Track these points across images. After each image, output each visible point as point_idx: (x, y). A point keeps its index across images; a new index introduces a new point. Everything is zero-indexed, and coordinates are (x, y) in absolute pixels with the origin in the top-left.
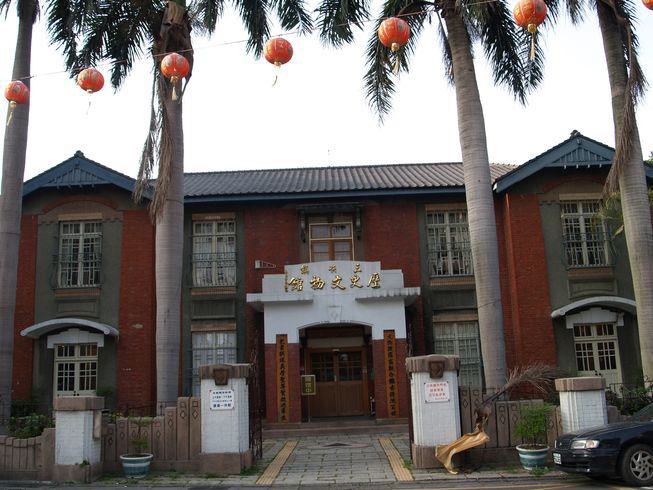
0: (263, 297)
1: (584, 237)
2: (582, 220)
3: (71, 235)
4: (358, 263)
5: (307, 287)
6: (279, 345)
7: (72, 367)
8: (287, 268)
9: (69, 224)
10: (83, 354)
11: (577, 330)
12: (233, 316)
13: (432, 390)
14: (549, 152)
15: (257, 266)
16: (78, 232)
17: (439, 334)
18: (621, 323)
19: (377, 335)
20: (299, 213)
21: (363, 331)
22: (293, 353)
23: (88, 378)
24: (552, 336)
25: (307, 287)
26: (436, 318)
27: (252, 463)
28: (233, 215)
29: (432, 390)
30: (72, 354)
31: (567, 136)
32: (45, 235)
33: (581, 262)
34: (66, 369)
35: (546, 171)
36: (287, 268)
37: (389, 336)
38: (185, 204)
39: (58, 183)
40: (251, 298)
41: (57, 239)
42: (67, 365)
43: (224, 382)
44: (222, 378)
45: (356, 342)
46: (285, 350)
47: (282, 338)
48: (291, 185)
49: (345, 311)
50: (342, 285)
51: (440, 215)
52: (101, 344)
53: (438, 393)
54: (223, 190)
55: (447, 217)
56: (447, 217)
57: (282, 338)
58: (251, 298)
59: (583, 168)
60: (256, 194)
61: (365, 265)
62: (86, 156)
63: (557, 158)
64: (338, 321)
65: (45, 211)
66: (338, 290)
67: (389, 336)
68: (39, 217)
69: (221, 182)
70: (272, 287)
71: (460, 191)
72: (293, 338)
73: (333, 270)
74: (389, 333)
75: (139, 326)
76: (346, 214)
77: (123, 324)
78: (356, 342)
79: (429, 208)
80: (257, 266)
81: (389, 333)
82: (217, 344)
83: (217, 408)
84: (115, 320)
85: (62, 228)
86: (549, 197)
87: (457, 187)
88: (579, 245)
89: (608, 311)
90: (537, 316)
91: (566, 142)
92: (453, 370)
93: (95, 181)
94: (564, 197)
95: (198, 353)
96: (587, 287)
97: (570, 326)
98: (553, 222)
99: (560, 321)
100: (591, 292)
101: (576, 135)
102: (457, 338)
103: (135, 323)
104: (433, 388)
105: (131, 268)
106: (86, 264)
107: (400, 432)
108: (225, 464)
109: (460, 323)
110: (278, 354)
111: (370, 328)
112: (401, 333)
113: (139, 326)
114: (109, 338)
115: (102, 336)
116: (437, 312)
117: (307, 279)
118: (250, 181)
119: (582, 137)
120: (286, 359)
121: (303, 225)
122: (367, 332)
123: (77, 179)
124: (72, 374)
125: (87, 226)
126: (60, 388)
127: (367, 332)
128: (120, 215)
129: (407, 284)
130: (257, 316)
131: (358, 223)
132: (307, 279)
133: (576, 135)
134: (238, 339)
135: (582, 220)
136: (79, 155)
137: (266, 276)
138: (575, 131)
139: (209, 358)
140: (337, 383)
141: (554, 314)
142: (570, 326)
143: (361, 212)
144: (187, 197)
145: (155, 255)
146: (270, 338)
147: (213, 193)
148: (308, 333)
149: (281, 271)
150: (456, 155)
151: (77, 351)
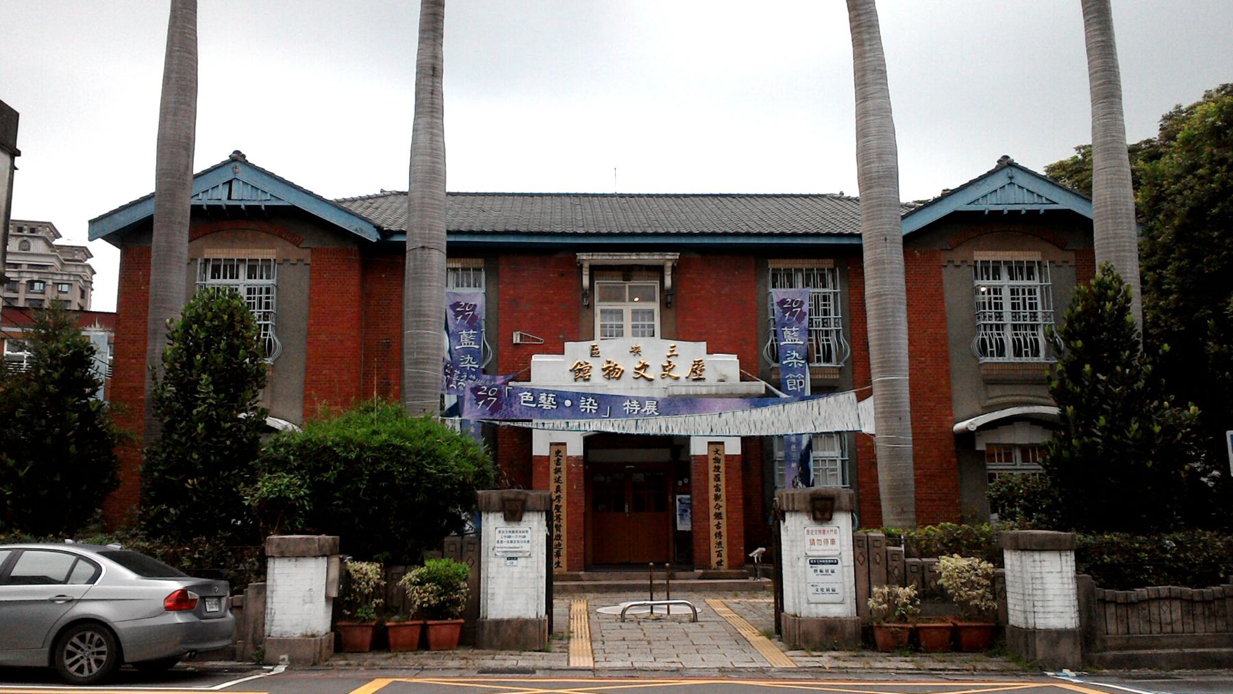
1: (1007, 319)
2: (1006, 293)
4: (673, 343)
6: (554, 459)
11: (988, 455)
15: (516, 338)
19: (698, 448)
21: (678, 445)
24: (954, 460)
28: (479, 262)
31: (992, 166)
35: (956, 218)
36: (567, 345)
43: (827, 515)
44: (822, 509)
45: (663, 455)
46: (563, 466)
47: (558, 447)
48: (385, 220)
50: (674, 374)
57: (558, 447)
59: (1014, 214)
60: (516, 233)
63: (985, 192)
67: (558, 452)
71: (855, 241)
73: (636, 351)
79: (772, 264)
80: (516, 338)
84: (297, 413)
86: (959, 255)
87: (851, 235)
90: (931, 430)
92: (846, 511)
93: (261, 200)
99: (967, 437)
105: (323, 337)
106: (1015, 327)
107: (755, 589)
117: (597, 366)
119: (1016, 166)
123: (242, 196)
128: (305, 254)
132: (597, 366)
135: (1006, 293)
137: (536, 358)
138: (1006, 157)
140: (638, 515)
141: (959, 426)
142: (981, 447)
144: (449, 233)
145: (864, 312)
150: (843, 179)
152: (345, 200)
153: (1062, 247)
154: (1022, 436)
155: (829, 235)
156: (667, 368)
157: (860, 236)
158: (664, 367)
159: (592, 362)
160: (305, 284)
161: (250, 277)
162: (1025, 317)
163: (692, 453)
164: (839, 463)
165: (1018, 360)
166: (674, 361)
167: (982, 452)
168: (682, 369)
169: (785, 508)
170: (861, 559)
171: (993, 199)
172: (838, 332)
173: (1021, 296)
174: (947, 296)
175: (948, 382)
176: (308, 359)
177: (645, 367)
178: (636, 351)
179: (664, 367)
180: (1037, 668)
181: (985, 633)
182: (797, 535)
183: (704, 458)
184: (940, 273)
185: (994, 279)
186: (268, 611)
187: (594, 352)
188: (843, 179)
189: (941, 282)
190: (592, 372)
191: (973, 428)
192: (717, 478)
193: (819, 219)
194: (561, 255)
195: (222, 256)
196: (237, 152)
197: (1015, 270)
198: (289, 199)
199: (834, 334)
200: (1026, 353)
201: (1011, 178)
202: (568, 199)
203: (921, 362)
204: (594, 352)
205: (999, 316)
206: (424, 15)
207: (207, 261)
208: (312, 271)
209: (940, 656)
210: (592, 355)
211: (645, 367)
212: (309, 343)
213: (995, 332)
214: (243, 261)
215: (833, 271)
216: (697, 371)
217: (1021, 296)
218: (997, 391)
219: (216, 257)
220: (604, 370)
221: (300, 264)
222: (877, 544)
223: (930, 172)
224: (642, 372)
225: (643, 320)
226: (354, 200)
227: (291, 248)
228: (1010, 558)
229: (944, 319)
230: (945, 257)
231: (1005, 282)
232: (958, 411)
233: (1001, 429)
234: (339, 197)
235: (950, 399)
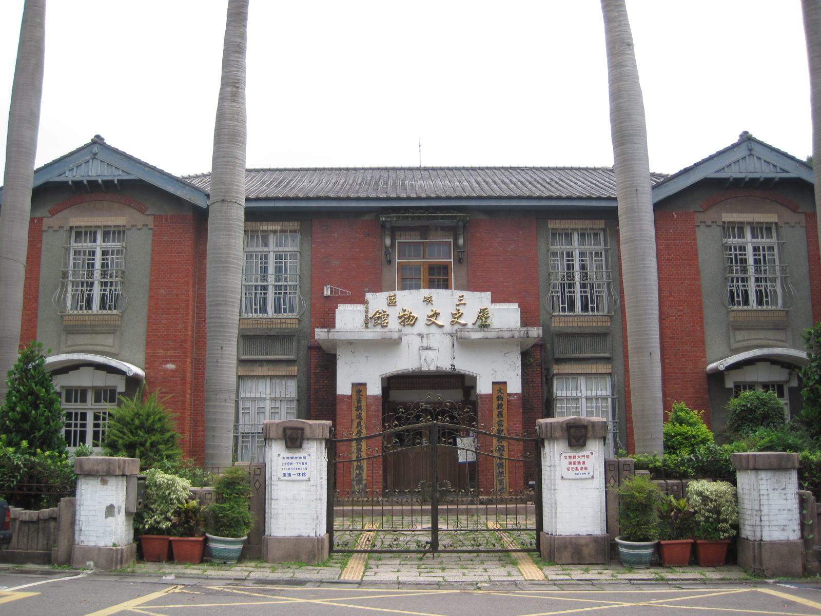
0: (334, 335)
3: (86, 245)
5: (393, 323)
6: (355, 397)
7: (84, 416)
8: (369, 296)
9: (83, 230)
10: (97, 400)
12: (292, 357)
13: (570, 463)
14: (711, 158)
15: (327, 292)
16: (95, 241)
17: (561, 391)
18: (794, 383)
19: (484, 388)
20: (383, 226)
21: (462, 383)
22: (373, 408)
23: (75, 432)
24: (707, 396)
25: (393, 323)
26: (556, 369)
27: (328, 549)
28: (296, 225)
29: (570, 463)
30: (84, 400)
31: (735, 139)
32: (51, 242)
33: (746, 302)
34: (76, 419)
36: (369, 296)
37: (500, 390)
38: (246, 208)
39: (70, 177)
40: (320, 334)
41: (67, 250)
42: (76, 414)
43: (581, 441)
45: (450, 397)
46: (363, 404)
47: (359, 388)
49: (440, 357)
50: (439, 322)
51: (119, 232)
52: (121, 388)
53: (579, 466)
54: (285, 192)
55: (576, 237)
56: (576, 237)
57: (359, 388)
58: (320, 334)
59: (753, 181)
60: (328, 198)
61: (468, 295)
62: (108, 142)
64: (433, 368)
65: (53, 213)
66: (424, 327)
67: (359, 392)
68: (45, 220)
69: (280, 183)
70: (349, 319)
72: (375, 389)
73: (428, 300)
74: (500, 386)
75: (171, 366)
76: (444, 229)
77: (148, 365)
78: (450, 397)
79: (553, 224)
80: (327, 292)
81: (500, 386)
82: (271, 398)
83: (287, 478)
84: (141, 357)
85: (73, 234)
86: (710, 215)
87: (609, 199)
88: (744, 280)
89: (779, 367)
90: (688, 371)
91: (734, 146)
93: (115, 175)
94: (728, 217)
95: (248, 405)
96: (753, 334)
97: (729, 384)
98: (708, 245)
99: (717, 377)
100: (746, 344)
101: (746, 138)
102: (268, 402)
103: (167, 362)
104: (572, 460)
105: (162, 291)
106: (757, 280)
108: (304, 552)
109: (586, 375)
110: (354, 409)
111: (474, 379)
112: (515, 386)
113: (171, 366)
114: (133, 382)
115: (124, 378)
116: (559, 361)
117: (394, 314)
118: (293, 184)
120: (364, 415)
121: (388, 242)
122: (467, 384)
123: (96, 171)
124: (83, 426)
125: (753, 230)
126: (604, 425)
127: (467, 384)
128: (150, 221)
129: (525, 322)
130: (324, 362)
131: (461, 242)
132: (394, 314)
133: (746, 138)
134: (299, 388)
136: (98, 141)
137: (341, 307)
138: (746, 133)
139: (261, 411)
142: (729, 384)
143: (464, 227)
144: (248, 200)
146: (343, 388)
147: (272, 195)
148: (392, 383)
149: (362, 301)
150: (602, 155)
151: (90, 396)
152: (190, 177)
153: (142, 212)
154: (762, 374)
155: (599, 198)
156: (457, 316)
157: (616, 199)
158: (453, 315)
159: (390, 311)
160: (148, 247)
161: (104, 241)
162: (765, 270)
163: (478, 392)
164: (610, 400)
165: (759, 307)
166: (462, 309)
167: (730, 389)
168: (469, 318)
169: (543, 436)
170: (612, 481)
171: (735, 168)
172: (609, 284)
173: (761, 253)
174: (700, 255)
175: (702, 327)
176: (150, 310)
177: (436, 315)
178: (428, 300)
179: (453, 315)
180: (759, 574)
181: (720, 547)
182: (556, 459)
183: (489, 397)
184: (694, 232)
185: (739, 237)
186: (77, 522)
187: (392, 303)
188: (602, 155)
189: (695, 240)
190: (390, 320)
191: (722, 368)
192: (500, 414)
193: (593, 186)
194: (367, 217)
195: (83, 224)
196: (98, 136)
197: (758, 229)
198: (135, 174)
199: (605, 286)
200: (767, 302)
201: (751, 150)
202: (378, 172)
203: (681, 311)
204: (392, 303)
205: (745, 270)
206: (41, 25)
207: (71, 228)
208: (154, 235)
209: (680, 570)
210: (389, 305)
211: (436, 315)
212: (151, 297)
213: (740, 284)
214: (99, 227)
215: (604, 230)
216: (483, 315)
217: (761, 253)
218: (740, 335)
219: (78, 224)
220: (400, 317)
221: (145, 228)
222: (626, 468)
223: (676, 147)
224: (433, 319)
225: (439, 275)
226: (197, 177)
227: (137, 214)
228: (741, 478)
229: (698, 273)
230: (699, 217)
231: (749, 241)
232: (710, 354)
233: (747, 368)
234: (185, 175)
235: (703, 342)
